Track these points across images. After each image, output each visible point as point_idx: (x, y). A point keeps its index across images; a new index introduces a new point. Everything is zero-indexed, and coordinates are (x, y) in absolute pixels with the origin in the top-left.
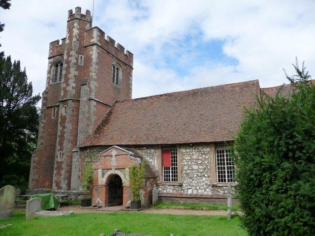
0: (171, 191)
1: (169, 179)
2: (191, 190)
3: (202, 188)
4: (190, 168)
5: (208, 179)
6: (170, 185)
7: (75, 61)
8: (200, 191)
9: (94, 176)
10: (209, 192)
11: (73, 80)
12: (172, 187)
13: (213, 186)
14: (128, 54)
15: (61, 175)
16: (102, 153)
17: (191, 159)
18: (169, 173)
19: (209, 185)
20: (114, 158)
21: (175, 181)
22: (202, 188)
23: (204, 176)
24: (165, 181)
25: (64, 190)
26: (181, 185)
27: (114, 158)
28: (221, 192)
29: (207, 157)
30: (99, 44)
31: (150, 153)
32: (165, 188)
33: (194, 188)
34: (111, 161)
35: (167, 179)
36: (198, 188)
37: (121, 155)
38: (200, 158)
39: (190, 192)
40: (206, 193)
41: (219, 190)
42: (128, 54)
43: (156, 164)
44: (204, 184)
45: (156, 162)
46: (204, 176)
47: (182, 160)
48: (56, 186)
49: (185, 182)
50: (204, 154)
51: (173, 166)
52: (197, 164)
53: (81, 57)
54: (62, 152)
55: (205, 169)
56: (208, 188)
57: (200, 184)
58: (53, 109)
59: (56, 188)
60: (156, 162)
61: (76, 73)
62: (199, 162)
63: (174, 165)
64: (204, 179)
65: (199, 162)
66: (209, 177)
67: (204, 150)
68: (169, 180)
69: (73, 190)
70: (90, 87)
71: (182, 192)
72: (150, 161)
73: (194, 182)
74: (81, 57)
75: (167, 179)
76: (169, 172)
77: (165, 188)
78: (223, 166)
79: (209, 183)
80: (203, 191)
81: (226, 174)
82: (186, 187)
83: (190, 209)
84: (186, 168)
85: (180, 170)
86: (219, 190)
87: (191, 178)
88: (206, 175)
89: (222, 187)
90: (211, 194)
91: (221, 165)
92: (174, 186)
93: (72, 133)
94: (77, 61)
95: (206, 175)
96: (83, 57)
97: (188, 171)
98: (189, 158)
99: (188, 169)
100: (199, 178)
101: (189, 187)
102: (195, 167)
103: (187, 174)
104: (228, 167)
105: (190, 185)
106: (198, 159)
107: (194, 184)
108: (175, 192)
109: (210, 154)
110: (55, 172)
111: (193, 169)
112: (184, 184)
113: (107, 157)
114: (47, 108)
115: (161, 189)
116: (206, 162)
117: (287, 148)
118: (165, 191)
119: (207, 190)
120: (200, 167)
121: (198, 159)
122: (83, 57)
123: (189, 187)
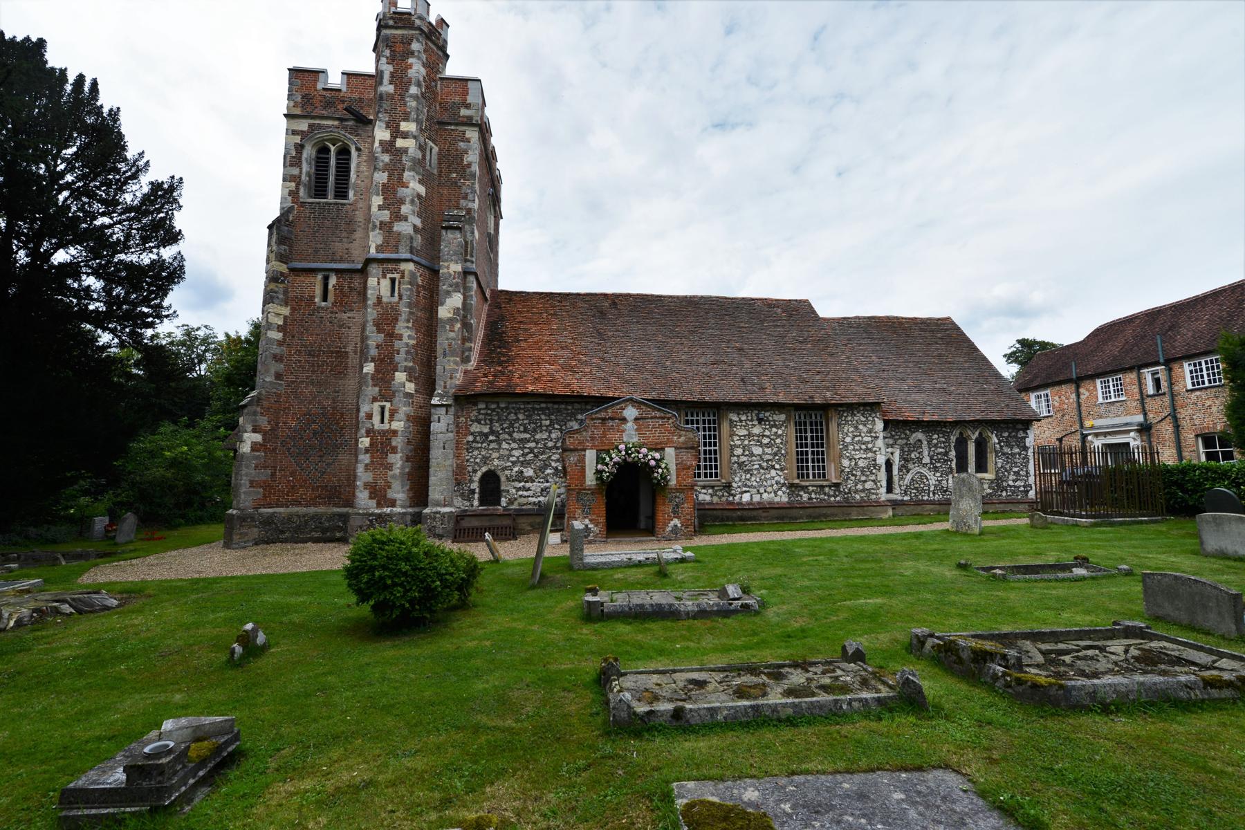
0: (708, 498)
1: (808, 474)
2: (748, 494)
3: (769, 489)
4: (747, 453)
5: (780, 473)
6: (704, 487)
8: (765, 496)
10: (783, 497)
12: (710, 491)
13: (791, 486)
15: (390, 467)
16: (597, 412)
17: (750, 435)
18: (807, 462)
19: (784, 485)
20: (630, 425)
21: (711, 476)
22: (769, 489)
23: (773, 467)
25: (402, 507)
26: (728, 486)
27: (630, 425)
28: (805, 497)
29: (780, 432)
33: (755, 491)
34: (623, 431)
36: (762, 490)
37: (652, 418)
38: (767, 433)
39: (746, 497)
40: (777, 499)
41: (802, 493)
44: (774, 482)
46: (773, 467)
47: (731, 436)
48: (371, 498)
49: (737, 479)
50: (775, 426)
52: (761, 445)
54: (388, 405)
55: (776, 454)
56: (780, 489)
57: (765, 483)
58: (320, 277)
59: (373, 503)
61: (422, 190)
62: (766, 441)
63: (818, 452)
64: (773, 472)
65: (766, 441)
66: (782, 469)
67: (775, 417)
68: (808, 477)
69: (438, 504)
71: (731, 498)
73: (753, 479)
75: (711, 474)
78: (713, 448)
79: (782, 481)
80: (773, 494)
81: (810, 464)
82: (739, 490)
83: (1009, 530)
84: (739, 451)
86: (802, 493)
87: (748, 471)
88: (777, 466)
89: (807, 486)
90: (787, 500)
91: (710, 451)
92: (713, 487)
93: (417, 354)
95: (777, 466)
97: (743, 459)
98: (746, 432)
99: (743, 455)
100: (762, 471)
101: (744, 489)
102: (757, 451)
103: (741, 465)
104: (813, 452)
105: (746, 486)
106: (763, 436)
107: (755, 483)
108: (715, 499)
109: (786, 427)
111: (752, 455)
112: (734, 485)
113: (611, 423)
114: (292, 270)
116: (778, 441)
119: (780, 493)
120: (768, 451)
121: (763, 436)
123: (744, 489)
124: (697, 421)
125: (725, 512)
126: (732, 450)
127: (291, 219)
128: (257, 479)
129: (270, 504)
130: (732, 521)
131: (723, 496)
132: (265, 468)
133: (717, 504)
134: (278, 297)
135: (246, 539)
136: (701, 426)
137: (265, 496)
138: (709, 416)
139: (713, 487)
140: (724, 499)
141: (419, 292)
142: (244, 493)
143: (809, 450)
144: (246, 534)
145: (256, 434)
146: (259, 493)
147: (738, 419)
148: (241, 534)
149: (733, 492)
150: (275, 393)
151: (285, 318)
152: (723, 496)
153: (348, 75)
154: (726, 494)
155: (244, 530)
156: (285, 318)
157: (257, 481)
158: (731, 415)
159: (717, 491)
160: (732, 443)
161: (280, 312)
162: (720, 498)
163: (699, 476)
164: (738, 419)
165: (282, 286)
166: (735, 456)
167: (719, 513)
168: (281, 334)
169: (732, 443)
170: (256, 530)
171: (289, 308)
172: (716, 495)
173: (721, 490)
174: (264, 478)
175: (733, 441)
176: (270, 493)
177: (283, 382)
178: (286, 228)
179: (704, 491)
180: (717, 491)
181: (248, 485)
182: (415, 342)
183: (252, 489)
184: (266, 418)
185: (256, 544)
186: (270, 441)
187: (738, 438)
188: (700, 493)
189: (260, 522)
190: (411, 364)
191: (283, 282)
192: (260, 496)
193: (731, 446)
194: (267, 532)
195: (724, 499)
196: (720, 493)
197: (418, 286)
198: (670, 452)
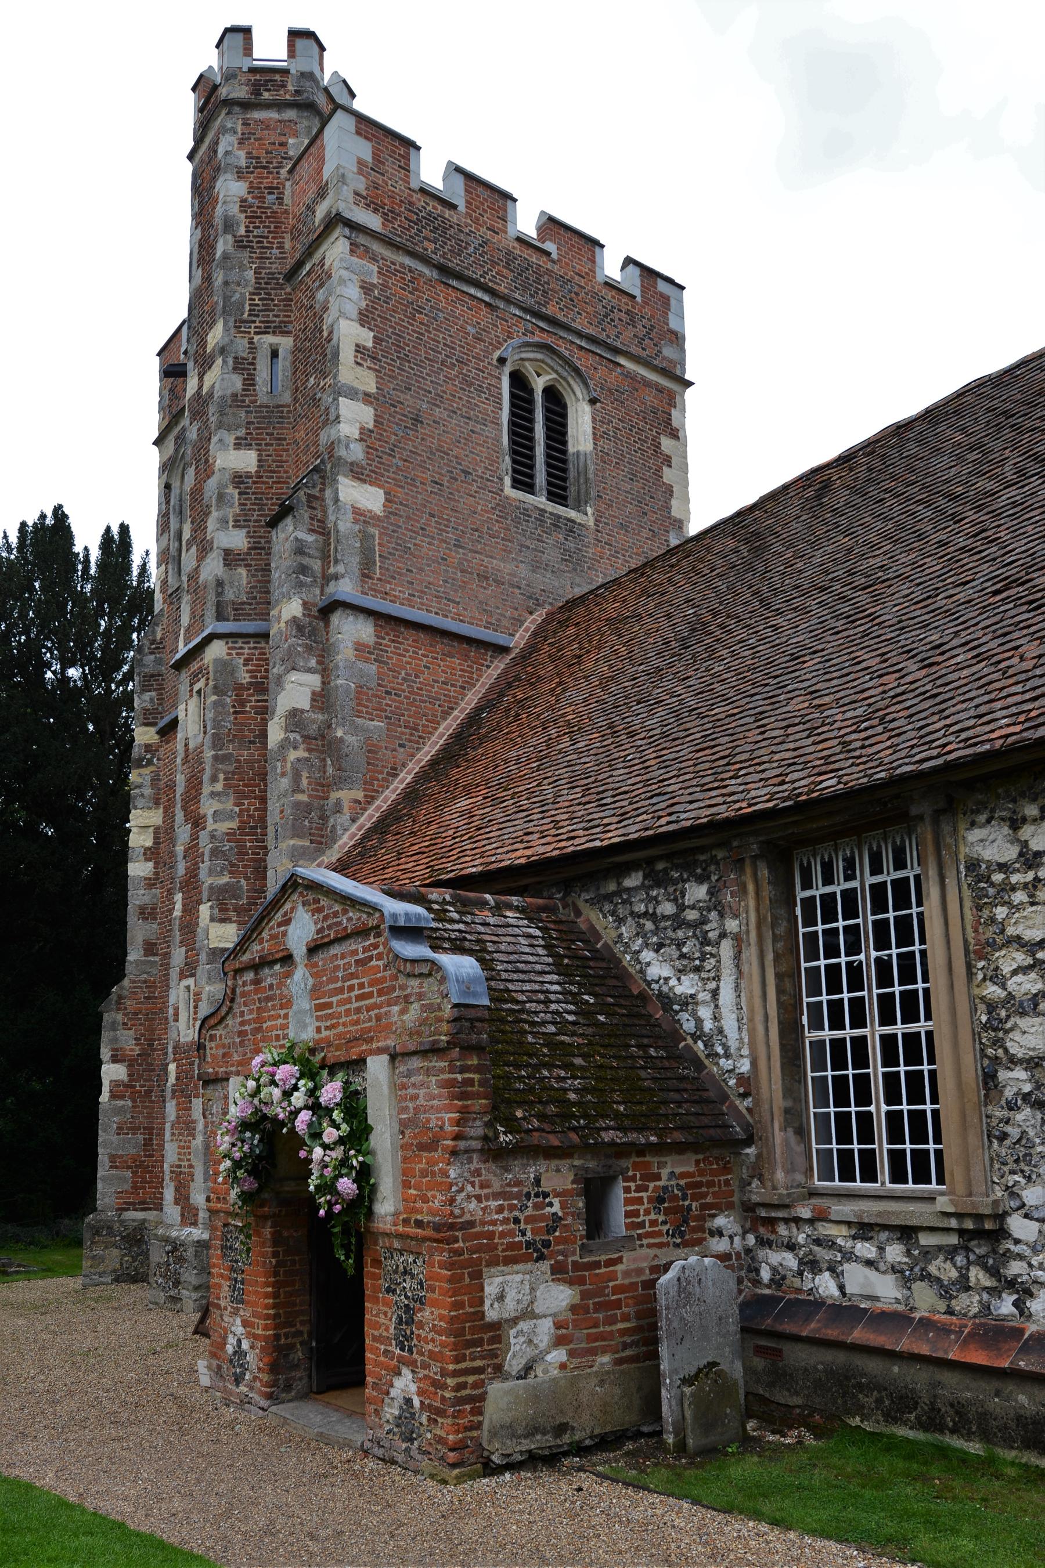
1: (868, 1159)
6: (864, 1230)
7: (237, 382)
9: (799, 1138)
11: (232, 511)
12: (895, 1252)
14: (633, 284)
24: (898, 1176)
27: (300, 978)
30: (373, 221)
31: (678, 921)
32: (824, 1254)
35: (846, 1157)
42: (633, 284)
43: (730, 1023)
45: (727, 995)
47: (985, 949)
48: (176, 1203)
51: (899, 1029)
53: (275, 354)
60: (727, 995)
63: (837, 1023)
70: (322, 528)
71: (1006, 1306)
72: (686, 986)
74: (275, 354)
76: (863, 1083)
77: (824, 1254)
85: (969, 1059)
92: (907, 1233)
94: (250, 382)
96: (285, 343)
110: (171, 1109)
115: (790, 1261)
117: (1011, 1284)
118: (826, 1285)
122: (285, 343)
124: (849, 897)
125: (950, 1378)
126: (997, 1027)
127: (159, 636)
128: (121, 1152)
129: (144, 1203)
130: (986, 1436)
131: (964, 1284)
132: (134, 1130)
133: (925, 1324)
134: (142, 795)
135: (101, 1269)
136: (867, 919)
137: (135, 1187)
138: (900, 864)
139: (907, 1233)
140: (969, 1303)
141: (242, 703)
142: (103, 1178)
143: (874, 1032)
144: (102, 1259)
145: (117, 1066)
146: (124, 1179)
147: (1010, 853)
148: (94, 1257)
149: (1015, 1268)
150: (145, 982)
151: (157, 830)
152: (964, 1284)
153: (551, 225)
154: (977, 1275)
155: (98, 1251)
156: (157, 830)
157: (122, 1156)
158: (974, 835)
159: (928, 1254)
160: (993, 991)
161: (146, 822)
162: (946, 1292)
163: (870, 1174)
164: (1010, 853)
165: (146, 771)
166: (1013, 1061)
167: (919, 1378)
168: (151, 864)
169: (993, 991)
170: (116, 1252)
171: (161, 810)
172: (926, 1276)
173: (950, 1253)
174: (133, 1151)
175: (996, 977)
176: (144, 1181)
177: (157, 959)
178: (152, 657)
179: (866, 1249)
180: (928, 1254)
181: (108, 1164)
182: (234, 824)
183: (113, 1172)
184: (131, 1032)
185: (117, 1280)
186: (140, 1076)
187: (1021, 958)
188: (849, 1256)
189: (123, 1238)
190: (225, 879)
191: (150, 762)
192: (127, 1186)
193: (991, 1007)
194: (134, 1259)
195: (969, 1303)
196: (945, 1270)
197: (239, 688)
198: (377, 1067)
